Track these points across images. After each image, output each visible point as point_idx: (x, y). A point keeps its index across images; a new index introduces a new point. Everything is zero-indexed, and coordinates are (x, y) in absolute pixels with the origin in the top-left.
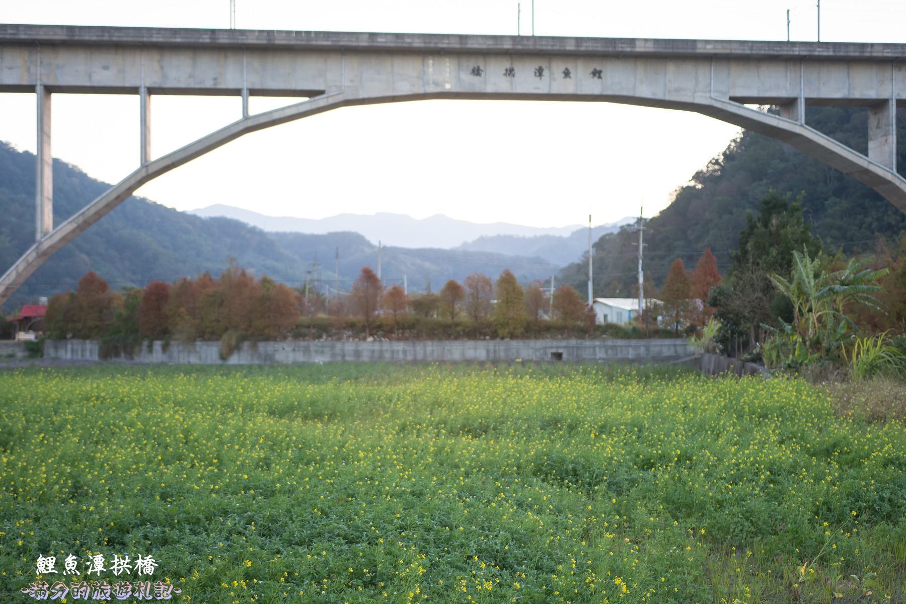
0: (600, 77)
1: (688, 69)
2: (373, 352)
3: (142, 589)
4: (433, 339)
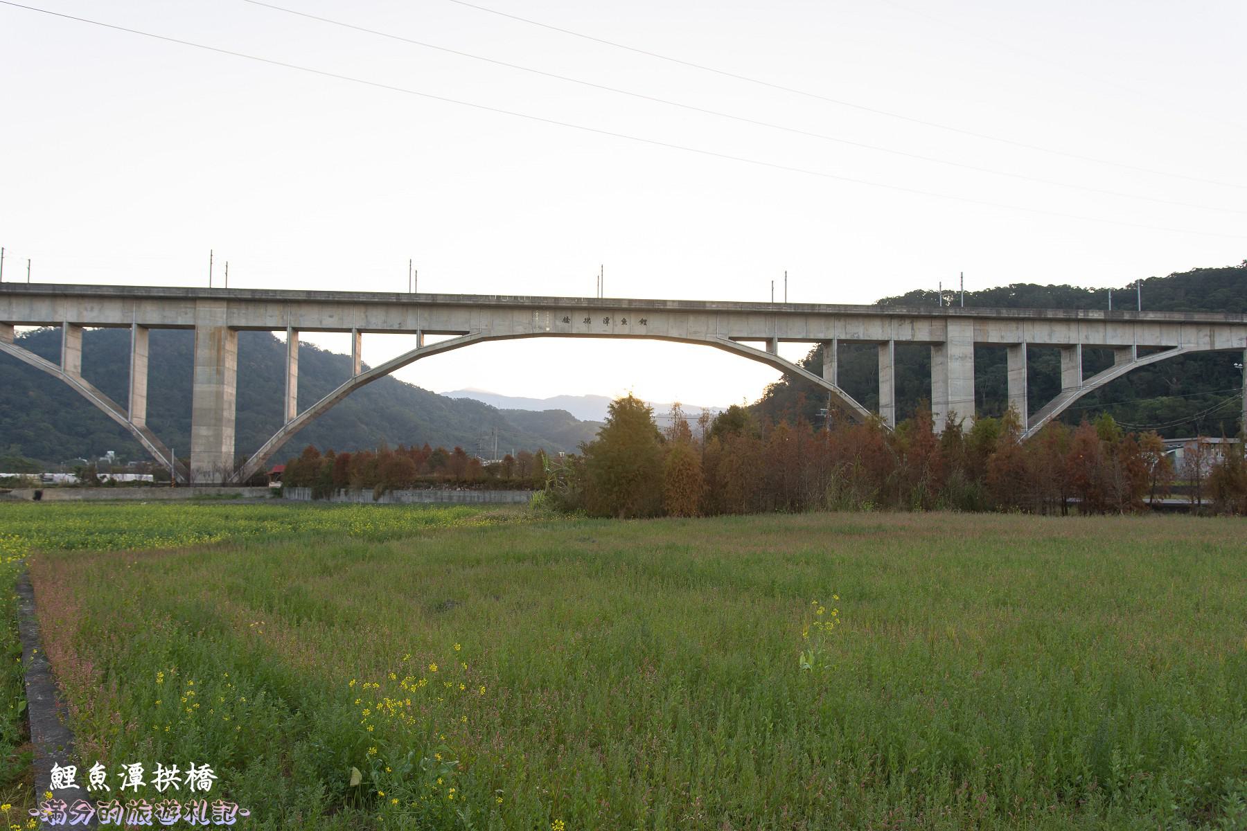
0: (645, 324)
1: (703, 318)
2: (460, 496)
3: (195, 810)
4: (496, 490)
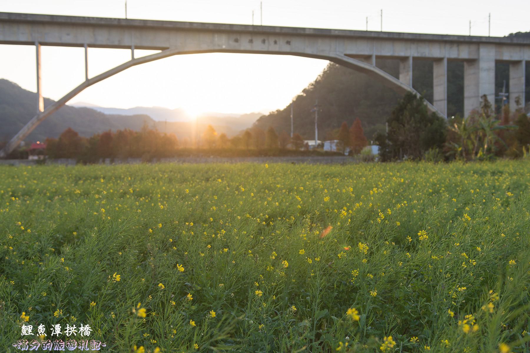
0: (290, 44)
3: (83, 344)
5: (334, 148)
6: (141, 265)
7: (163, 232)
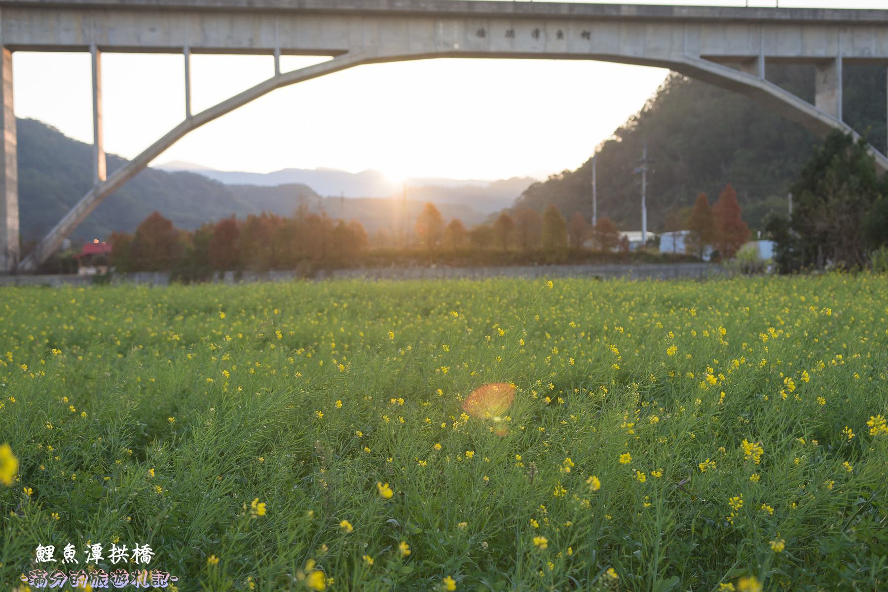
0: (589, 38)
5: (681, 247)
6: (299, 483)
7: (343, 419)
